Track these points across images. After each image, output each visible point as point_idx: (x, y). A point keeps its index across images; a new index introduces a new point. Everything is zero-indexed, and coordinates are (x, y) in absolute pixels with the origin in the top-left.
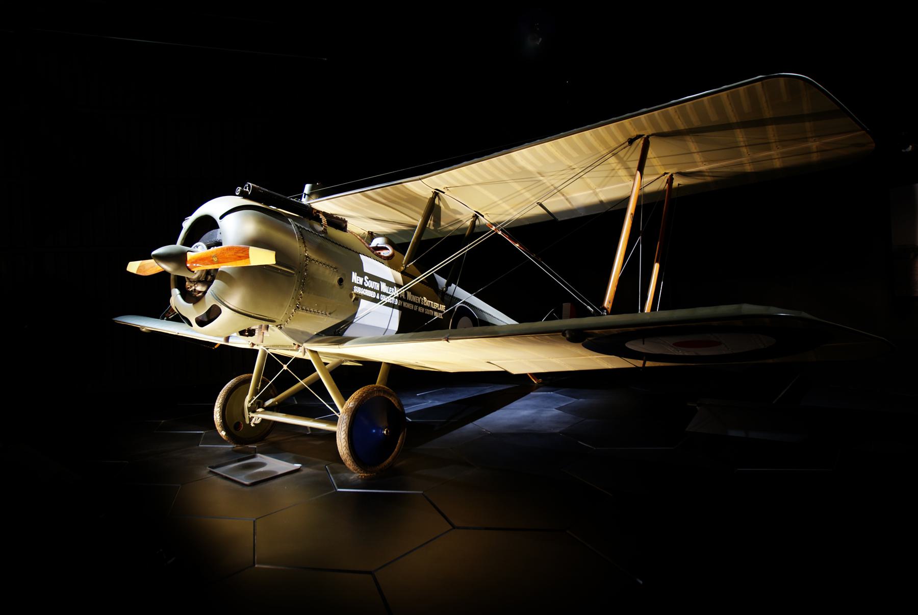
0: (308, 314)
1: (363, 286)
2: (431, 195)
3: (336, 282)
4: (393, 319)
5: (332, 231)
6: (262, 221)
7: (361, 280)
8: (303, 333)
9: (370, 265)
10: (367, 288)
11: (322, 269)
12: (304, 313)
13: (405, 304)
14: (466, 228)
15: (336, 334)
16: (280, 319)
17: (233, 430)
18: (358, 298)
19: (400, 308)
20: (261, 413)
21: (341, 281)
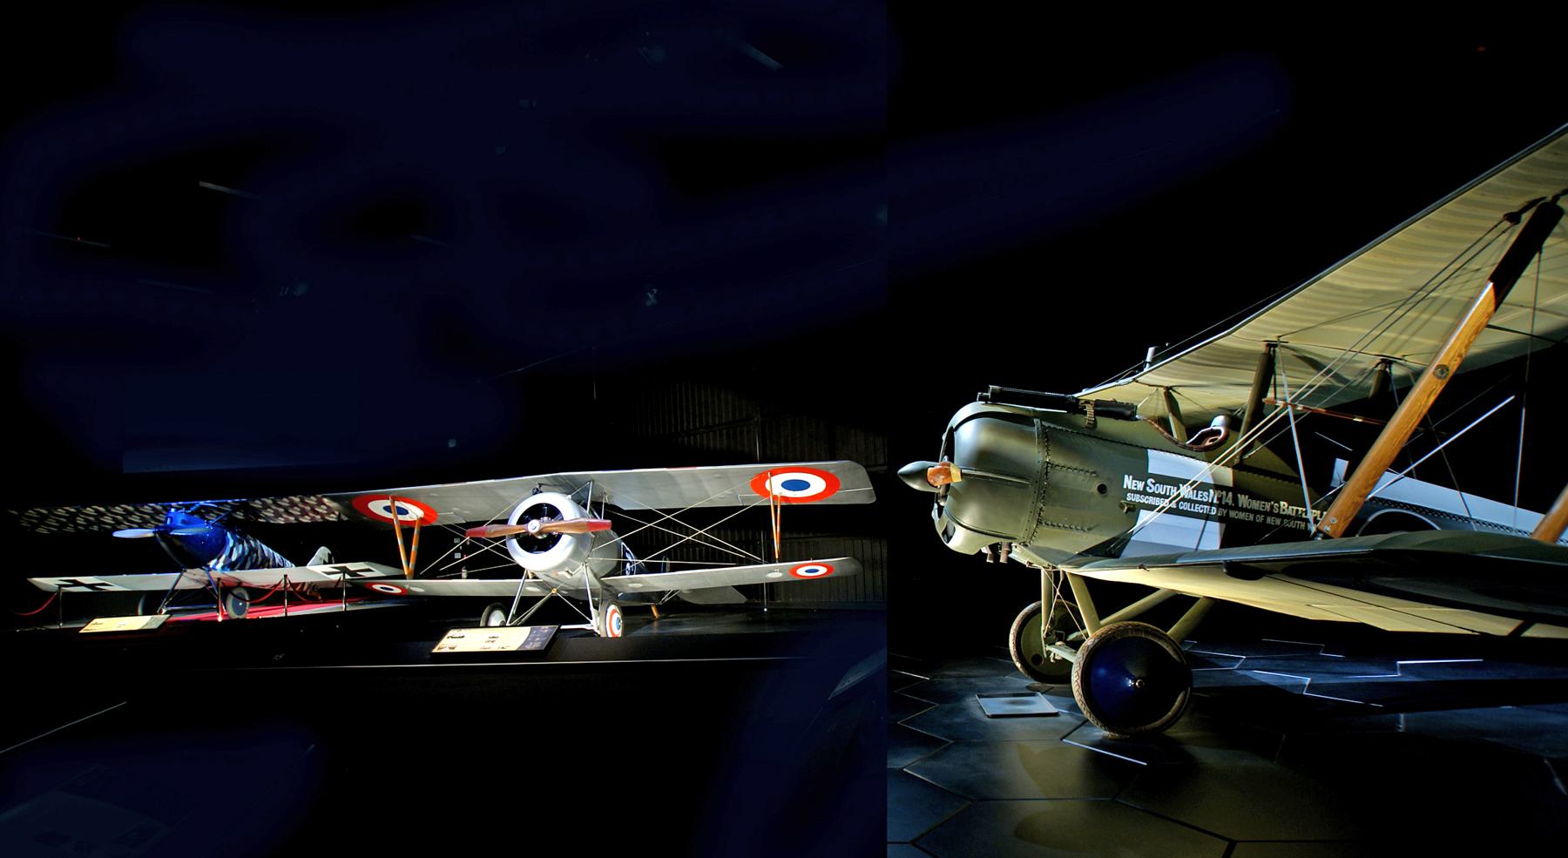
0: (1056, 530)
1: (1144, 493)
2: (1262, 348)
3: (1094, 489)
4: (1212, 537)
5: (1106, 424)
6: (993, 429)
7: (1140, 486)
8: (1058, 552)
9: (1159, 462)
10: (1153, 494)
11: (1071, 475)
12: (1050, 529)
13: (1232, 514)
14: (1368, 389)
15: (1110, 551)
16: (1021, 535)
17: (1029, 660)
18: (1134, 510)
19: (1220, 519)
20: (1059, 648)
21: (1102, 489)
